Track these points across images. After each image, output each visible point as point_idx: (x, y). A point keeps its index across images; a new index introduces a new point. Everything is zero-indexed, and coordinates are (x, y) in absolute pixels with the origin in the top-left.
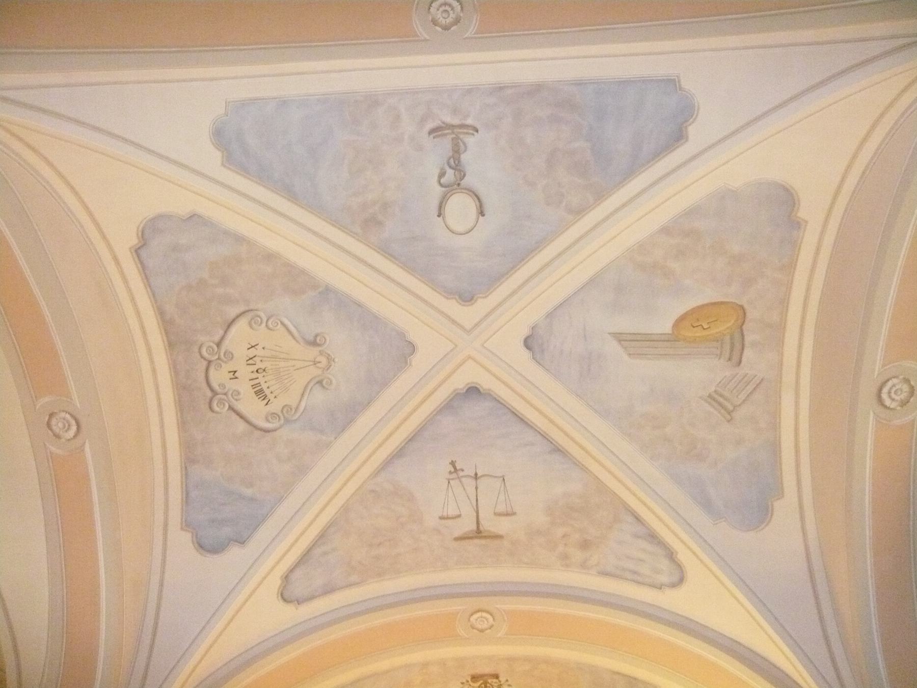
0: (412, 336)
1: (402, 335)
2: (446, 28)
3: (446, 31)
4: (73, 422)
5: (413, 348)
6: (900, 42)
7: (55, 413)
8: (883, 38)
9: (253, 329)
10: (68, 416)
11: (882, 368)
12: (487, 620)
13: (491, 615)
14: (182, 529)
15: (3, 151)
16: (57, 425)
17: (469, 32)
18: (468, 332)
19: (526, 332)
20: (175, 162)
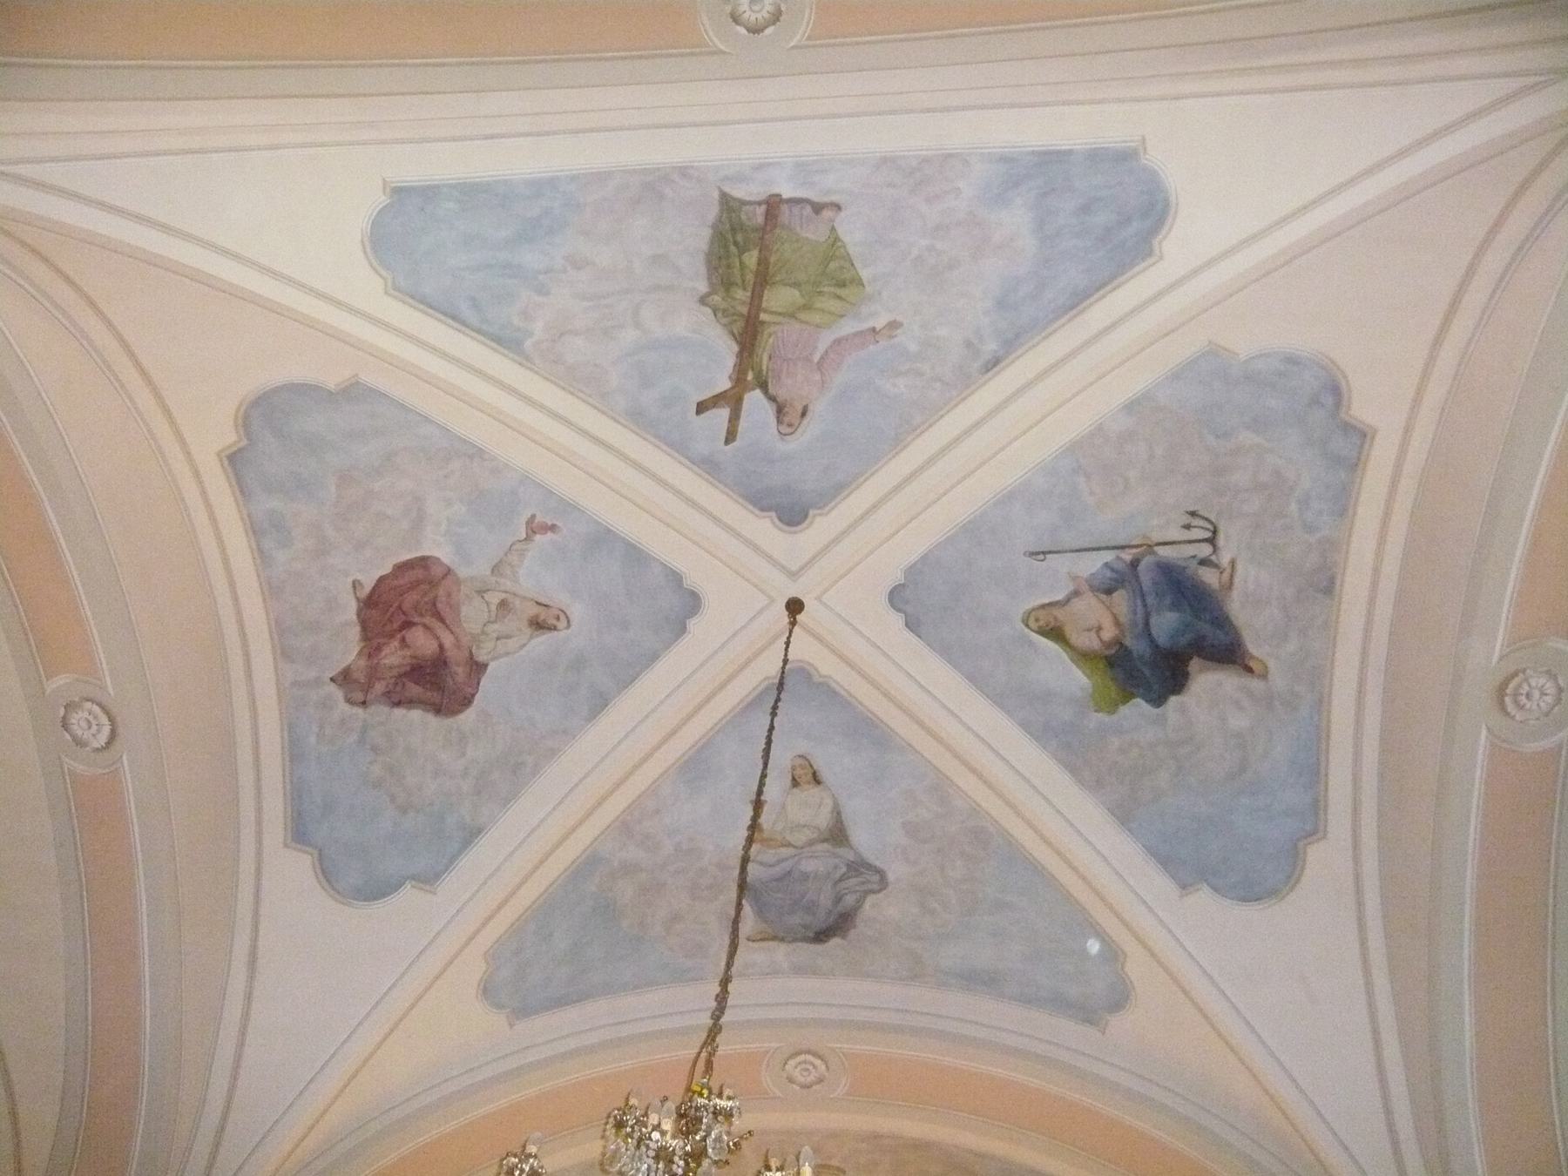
0: (694, 578)
1: (676, 578)
2: (755, 30)
3: (756, 35)
4: (104, 720)
5: (693, 602)
6: (1532, 80)
7: (733, 10)
8: (1506, 75)
9: (799, 756)
10: (96, 709)
11: (1507, 647)
12: (815, 1067)
13: (820, 1057)
14: (286, 845)
15: (5, 274)
16: (77, 719)
17: (798, 37)
18: (794, 575)
19: (897, 577)
20: (257, 902)
